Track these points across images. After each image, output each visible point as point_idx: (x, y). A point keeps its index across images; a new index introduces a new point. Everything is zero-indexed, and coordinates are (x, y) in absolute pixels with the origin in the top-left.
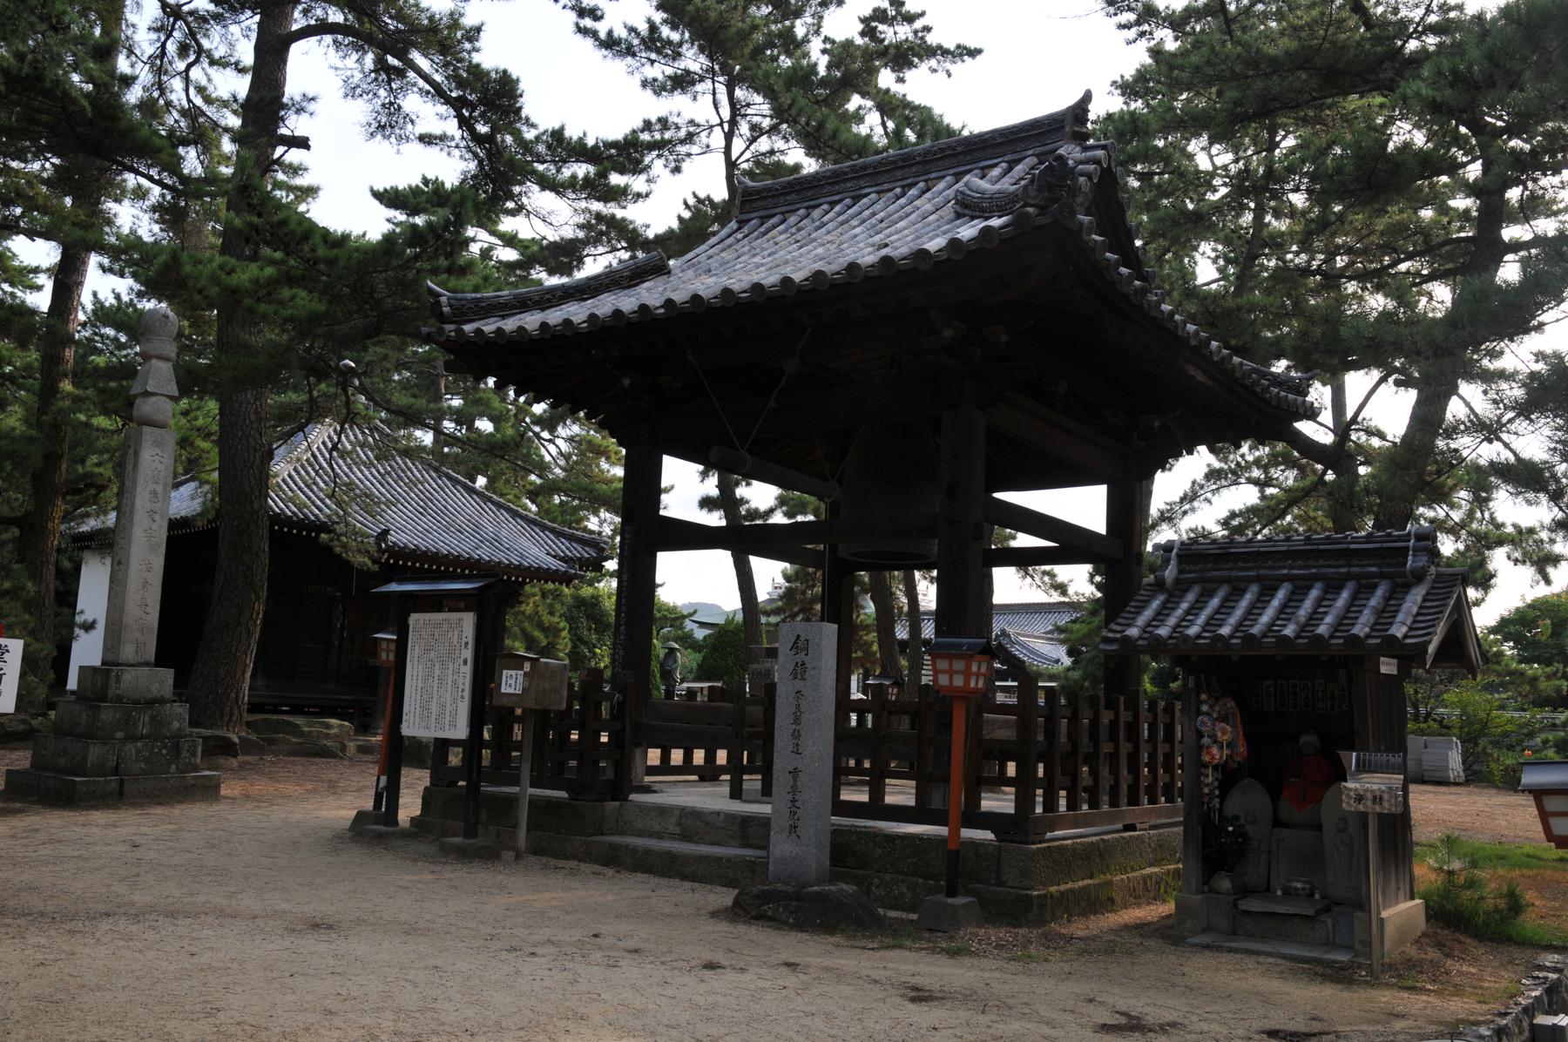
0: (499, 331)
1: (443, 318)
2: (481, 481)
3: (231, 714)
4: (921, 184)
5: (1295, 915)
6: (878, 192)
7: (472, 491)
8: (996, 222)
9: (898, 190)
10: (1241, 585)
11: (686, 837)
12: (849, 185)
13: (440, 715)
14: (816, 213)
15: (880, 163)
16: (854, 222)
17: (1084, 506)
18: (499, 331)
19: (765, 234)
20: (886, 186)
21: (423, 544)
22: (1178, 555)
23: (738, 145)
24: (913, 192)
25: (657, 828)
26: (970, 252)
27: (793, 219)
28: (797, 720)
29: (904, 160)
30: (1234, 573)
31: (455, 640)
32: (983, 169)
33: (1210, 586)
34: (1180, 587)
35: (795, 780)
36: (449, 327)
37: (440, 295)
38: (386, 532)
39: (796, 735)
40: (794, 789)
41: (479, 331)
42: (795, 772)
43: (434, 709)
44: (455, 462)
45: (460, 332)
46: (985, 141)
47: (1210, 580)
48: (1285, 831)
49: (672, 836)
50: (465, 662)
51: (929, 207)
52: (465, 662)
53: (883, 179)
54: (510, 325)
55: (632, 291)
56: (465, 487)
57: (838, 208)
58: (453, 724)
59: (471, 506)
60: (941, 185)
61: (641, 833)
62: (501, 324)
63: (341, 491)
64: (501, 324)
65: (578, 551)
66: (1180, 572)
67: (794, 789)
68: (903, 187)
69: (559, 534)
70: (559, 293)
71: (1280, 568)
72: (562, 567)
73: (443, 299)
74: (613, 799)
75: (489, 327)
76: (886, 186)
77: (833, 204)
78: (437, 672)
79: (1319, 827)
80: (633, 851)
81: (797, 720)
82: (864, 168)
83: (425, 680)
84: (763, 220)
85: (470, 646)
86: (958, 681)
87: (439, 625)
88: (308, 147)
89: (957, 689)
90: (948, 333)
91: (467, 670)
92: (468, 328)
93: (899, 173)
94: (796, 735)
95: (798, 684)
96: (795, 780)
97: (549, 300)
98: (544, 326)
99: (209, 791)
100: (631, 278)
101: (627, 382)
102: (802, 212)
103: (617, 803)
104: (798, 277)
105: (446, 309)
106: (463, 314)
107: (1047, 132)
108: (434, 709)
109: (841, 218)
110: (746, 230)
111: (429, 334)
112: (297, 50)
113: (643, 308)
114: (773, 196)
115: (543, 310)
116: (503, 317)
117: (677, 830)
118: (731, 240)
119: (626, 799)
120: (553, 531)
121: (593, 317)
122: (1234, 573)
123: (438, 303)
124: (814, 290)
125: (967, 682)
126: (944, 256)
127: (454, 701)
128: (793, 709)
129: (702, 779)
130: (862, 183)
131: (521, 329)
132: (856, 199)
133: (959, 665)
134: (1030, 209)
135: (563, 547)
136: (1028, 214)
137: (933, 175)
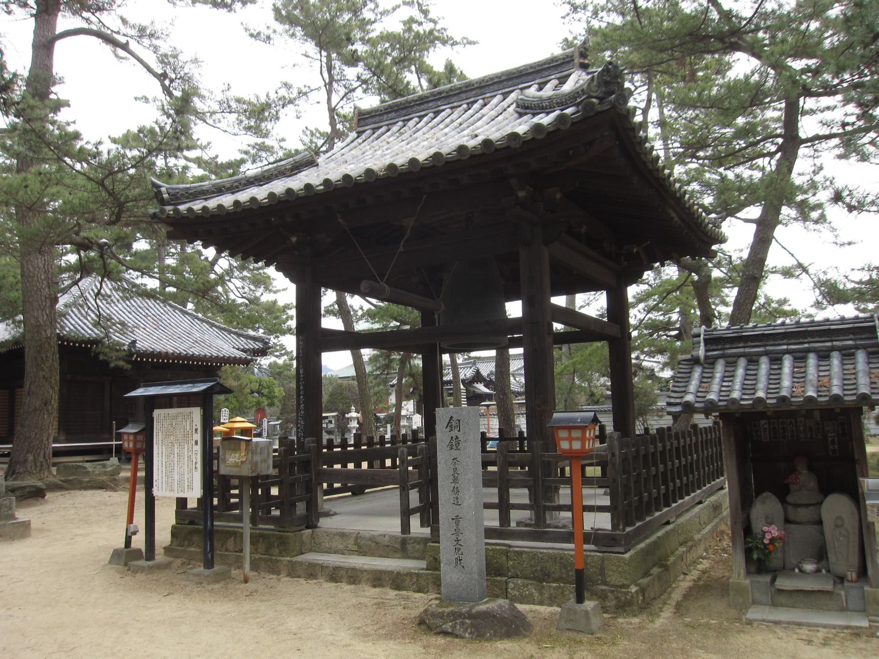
0: (205, 208)
1: (162, 202)
2: (190, 306)
3: (42, 465)
4: (481, 101)
5: (819, 591)
6: (451, 108)
7: (185, 313)
8: (569, 111)
9: (465, 106)
10: (754, 358)
11: (361, 551)
12: (430, 104)
13: (181, 481)
14: (411, 123)
15: (451, 90)
16: (441, 126)
17: (593, 304)
18: (205, 208)
19: (377, 139)
20: (455, 104)
21: (158, 347)
22: (705, 340)
23: (335, 99)
24: (476, 106)
25: (341, 547)
26: (549, 133)
27: (395, 128)
28: (455, 480)
29: (467, 87)
30: (747, 350)
31: (188, 428)
32: (521, 89)
33: (731, 359)
34: (710, 362)
35: (457, 525)
36: (169, 208)
37: (160, 187)
38: (134, 342)
39: (456, 491)
40: (457, 532)
41: (190, 210)
42: (457, 519)
43: (176, 477)
44: (173, 297)
45: (176, 211)
46: (521, 71)
47: (730, 356)
48: (792, 526)
49: (351, 552)
50: (196, 443)
51: (493, 113)
52: (196, 443)
53: (453, 99)
54: (212, 204)
55: (294, 178)
56: (181, 311)
57: (425, 119)
58: (190, 487)
59: (185, 321)
60: (495, 101)
61: (329, 551)
62: (205, 203)
63: (102, 321)
64: (205, 203)
65: (252, 345)
66: (706, 351)
67: (457, 532)
68: (468, 104)
69: (239, 335)
70: (243, 182)
71: (780, 345)
72: (244, 355)
73: (163, 189)
74: (308, 527)
75: (197, 206)
76: (455, 104)
77: (421, 118)
78: (176, 451)
79: (820, 522)
80: (323, 567)
81: (455, 480)
82: (440, 93)
83: (168, 456)
84: (374, 130)
85: (199, 431)
86: (577, 445)
87: (176, 417)
88: (69, 106)
89: (576, 451)
90: (521, 194)
91: (198, 448)
92: (182, 208)
93: (464, 96)
94: (456, 491)
95: (454, 453)
96: (457, 525)
97: (237, 187)
98: (237, 203)
99: (24, 530)
100: (292, 170)
101: (294, 239)
102: (400, 123)
103: (310, 530)
104: (421, 158)
105: (166, 196)
106: (178, 199)
107: (563, 63)
108: (176, 477)
109: (430, 125)
110: (363, 137)
111: (154, 214)
112: (59, 45)
113: (308, 187)
114: (380, 115)
115: (233, 193)
116: (206, 199)
117: (355, 548)
118: (355, 143)
119: (315, 527)
120: (235, 333)
121: (271, 195)
122: (747, 350)
123: (160, 192)
124: (434, 166)
125: (583, 445)
126: (530, 137)
127: (191, 471)
128: (452, 472)
129: (354, 494)
130: (439, 103)
131: (220, 207)
132: (437, 113)
133: (576, 434)
134: (594, 100)
135: (243, 343)
136: (593, 104)
137: (488, 95)
